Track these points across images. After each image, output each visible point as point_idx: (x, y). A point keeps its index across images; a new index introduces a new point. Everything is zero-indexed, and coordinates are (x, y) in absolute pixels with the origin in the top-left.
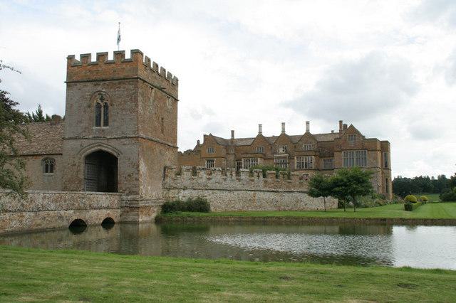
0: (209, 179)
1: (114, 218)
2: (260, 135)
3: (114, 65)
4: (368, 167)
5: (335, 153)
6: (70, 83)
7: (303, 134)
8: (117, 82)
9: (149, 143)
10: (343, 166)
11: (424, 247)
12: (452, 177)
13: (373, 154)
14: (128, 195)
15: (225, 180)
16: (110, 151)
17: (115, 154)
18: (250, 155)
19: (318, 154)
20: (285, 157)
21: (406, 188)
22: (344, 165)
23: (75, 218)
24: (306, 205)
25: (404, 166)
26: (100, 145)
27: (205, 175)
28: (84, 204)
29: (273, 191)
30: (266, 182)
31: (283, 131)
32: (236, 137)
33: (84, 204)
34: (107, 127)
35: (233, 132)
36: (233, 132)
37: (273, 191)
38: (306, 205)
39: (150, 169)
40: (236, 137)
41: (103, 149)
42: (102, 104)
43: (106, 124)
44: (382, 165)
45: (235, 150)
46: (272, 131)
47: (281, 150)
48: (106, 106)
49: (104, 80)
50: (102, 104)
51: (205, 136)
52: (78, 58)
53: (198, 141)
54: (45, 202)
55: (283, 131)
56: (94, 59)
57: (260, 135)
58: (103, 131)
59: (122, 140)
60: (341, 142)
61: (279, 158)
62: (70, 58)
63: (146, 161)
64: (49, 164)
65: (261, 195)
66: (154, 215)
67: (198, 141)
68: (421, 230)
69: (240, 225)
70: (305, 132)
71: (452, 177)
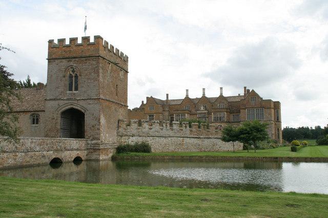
0: (151, 129)
1: (82, 157)
2: (187, 97)
3: (82, 47)
4: (265, 120)
5: (241, 110)
6: (50, 60)
7: (218, 96)
8: (84, 59)
9: (108, 103)
10: (247, 119)
11: (305, 178)
12: (325, 127)
13: (268, 111)
14: (92, 140)
15: (162, 129)
16: (79, 108)
17: (83, 111)
18: (180, 112)
19: (228, 110)
20: (205, 113)
21: (292, 136)
22: (248, 119)
23: (54, 157)
24: (220, 147)
25: (290, 119)
26: (72, 105)
27: (147, 126)
28: (61, 147)
29: (196, 138)
30: (191, 131)
31: (204, 94)
32: (169, 99)
33: (61, 147)
34: (77, 92)
35: (167, 95)
36: (167, 95)
37: (196, 138)
38: (220, 147)
39: (108, 122)
40: (169, 99)
41: (74, 107)
42: (74, 75)
43: (76, 89)
44: (275, 119)
45: (169, 108)
46: (195, 94)
47: (202, 108)
48: (76, 77)
49: (74, 58)
50: (74, 75)
51: (147, 98)
52: (56, 42)
53: (143, 102)
54: (33, 145)
55: (204, 94)
56: (67, 42)
57: (187, 97)
58: (74, 94)
59: (88, 101)
60: (245, 102)
61: (201, 113)
62: (51, 42)
63: (105, 116)
64: (35, 118)
65: (188, 140)
66: (111, 155)
67: (143, 102)
68: (303, 165)
69: (173, 162)
70: (219, 95)
71: (325, 127)
